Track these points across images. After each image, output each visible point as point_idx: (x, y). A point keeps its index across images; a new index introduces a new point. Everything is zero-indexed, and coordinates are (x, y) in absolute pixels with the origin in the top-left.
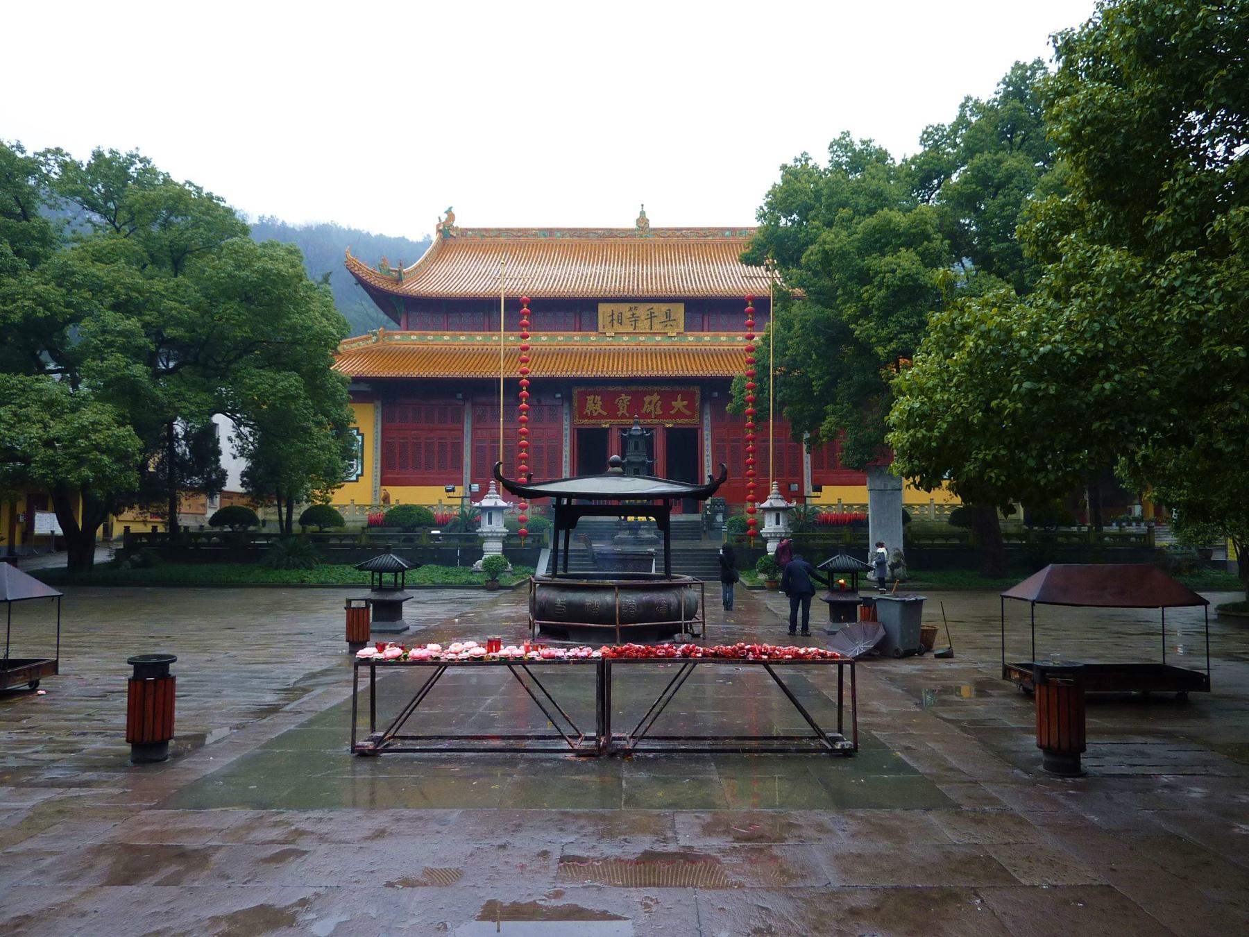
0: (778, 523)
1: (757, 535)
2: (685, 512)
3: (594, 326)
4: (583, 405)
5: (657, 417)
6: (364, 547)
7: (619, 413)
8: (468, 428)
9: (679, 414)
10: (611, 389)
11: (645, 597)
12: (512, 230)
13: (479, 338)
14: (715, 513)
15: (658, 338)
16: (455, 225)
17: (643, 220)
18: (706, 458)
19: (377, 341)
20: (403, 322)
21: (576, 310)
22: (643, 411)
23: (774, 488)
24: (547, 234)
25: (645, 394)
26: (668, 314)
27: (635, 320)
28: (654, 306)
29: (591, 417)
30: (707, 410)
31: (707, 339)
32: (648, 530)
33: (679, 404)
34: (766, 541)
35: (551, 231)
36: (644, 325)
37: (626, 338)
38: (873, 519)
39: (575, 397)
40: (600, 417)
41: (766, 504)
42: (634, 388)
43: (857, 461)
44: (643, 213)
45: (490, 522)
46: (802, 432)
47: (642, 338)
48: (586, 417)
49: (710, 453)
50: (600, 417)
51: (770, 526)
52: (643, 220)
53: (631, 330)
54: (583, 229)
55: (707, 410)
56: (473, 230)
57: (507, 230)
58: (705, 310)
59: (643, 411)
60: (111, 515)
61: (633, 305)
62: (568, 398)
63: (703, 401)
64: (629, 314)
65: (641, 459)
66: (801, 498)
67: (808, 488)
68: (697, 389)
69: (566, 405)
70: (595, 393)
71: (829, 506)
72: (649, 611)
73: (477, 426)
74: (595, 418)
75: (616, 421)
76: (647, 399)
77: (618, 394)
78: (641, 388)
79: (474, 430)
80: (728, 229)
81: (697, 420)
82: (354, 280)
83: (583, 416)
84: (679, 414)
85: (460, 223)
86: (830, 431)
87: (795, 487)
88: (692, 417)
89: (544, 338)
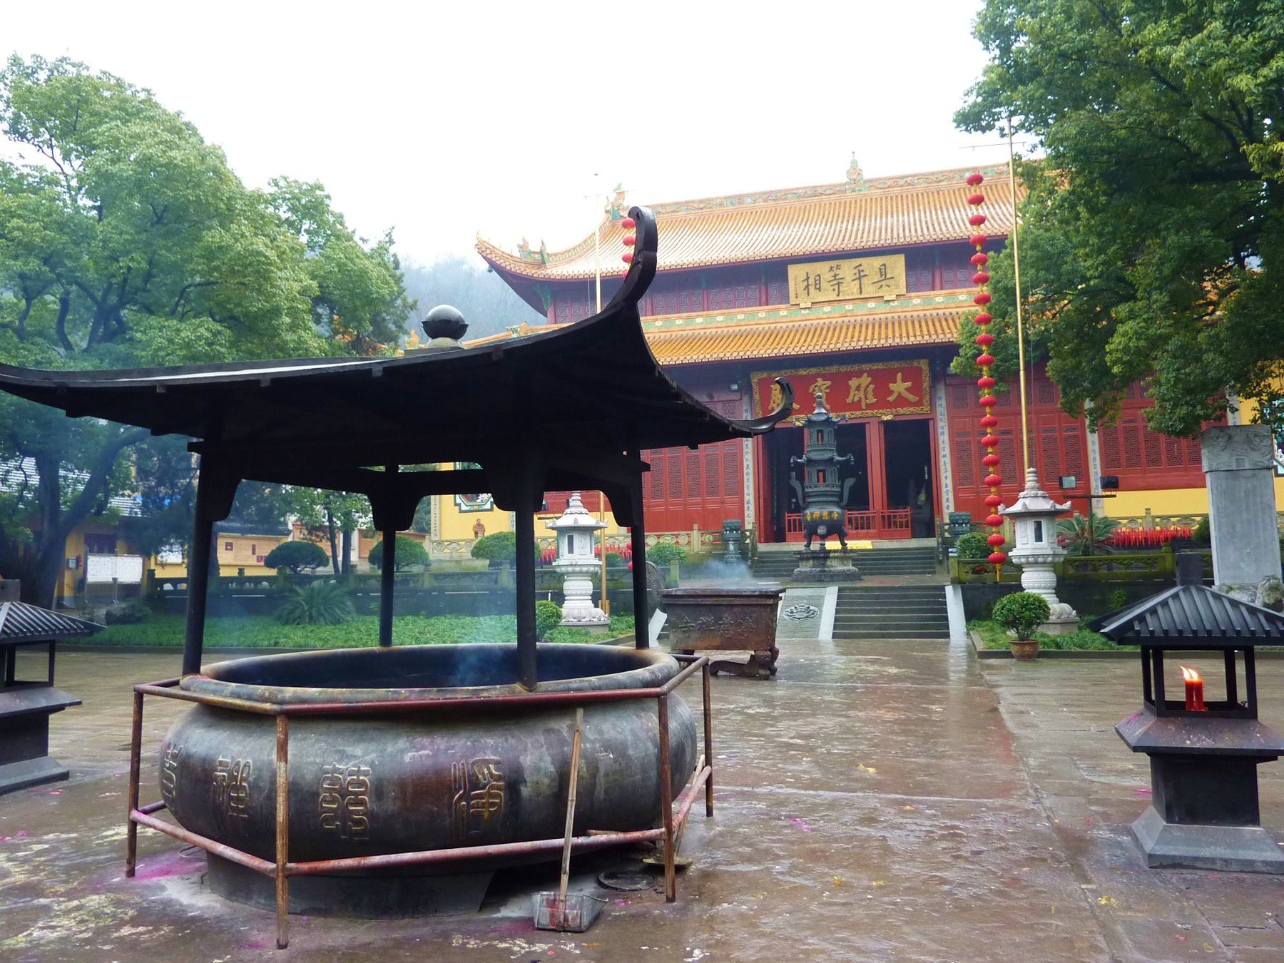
0: (1039, 538)
1: (1004, 560)
3: (784, 298)
5: (869, 407)
6: (428, 592)
9: (901, 401)
10: (803, 372)
11: (411, 753)
15: (871, 305)
17: (855, 170)
18: (942, 460)
22: (849, 400)
23: (1030, 478)
25: (850, 376)
26: (883, 271)
27: (838, 282)
28: (865, 262)
30: (941, 392)
32: (841, 559)
33: (899, 387)
35: (740, 198)
36: (850, 289)
37: (827, 309)
38: (1219, 527)
39: (755, 387)
41: (1017, 508)
42: (834, 369)
43: (1182, 419)
44: (854, 163)
45: (571, 550)
46: (1079, 399)
47: (849, 307)
51: (1024, 543)
52: (855, 170)
54: (780, 191)
55: (941, 392)
58: (931, 261)
59: (849, 400)
61: (834, 263)
62: (747, 389)
64: (829, 276)
65: (827, 456)
66: (1084, 500)
68: (924, 364)
69: (746, 399)
71: (1132, 520)
72: (425, 808)
76: (853, 383)
77: (812, 379)
78: (844, 369)
81: (927, 408)
82: (487, 265)
84: (901, 401)
86: (1126, 350)
87: (1070, 482)
88: (919, 404)
89: (720, 318)
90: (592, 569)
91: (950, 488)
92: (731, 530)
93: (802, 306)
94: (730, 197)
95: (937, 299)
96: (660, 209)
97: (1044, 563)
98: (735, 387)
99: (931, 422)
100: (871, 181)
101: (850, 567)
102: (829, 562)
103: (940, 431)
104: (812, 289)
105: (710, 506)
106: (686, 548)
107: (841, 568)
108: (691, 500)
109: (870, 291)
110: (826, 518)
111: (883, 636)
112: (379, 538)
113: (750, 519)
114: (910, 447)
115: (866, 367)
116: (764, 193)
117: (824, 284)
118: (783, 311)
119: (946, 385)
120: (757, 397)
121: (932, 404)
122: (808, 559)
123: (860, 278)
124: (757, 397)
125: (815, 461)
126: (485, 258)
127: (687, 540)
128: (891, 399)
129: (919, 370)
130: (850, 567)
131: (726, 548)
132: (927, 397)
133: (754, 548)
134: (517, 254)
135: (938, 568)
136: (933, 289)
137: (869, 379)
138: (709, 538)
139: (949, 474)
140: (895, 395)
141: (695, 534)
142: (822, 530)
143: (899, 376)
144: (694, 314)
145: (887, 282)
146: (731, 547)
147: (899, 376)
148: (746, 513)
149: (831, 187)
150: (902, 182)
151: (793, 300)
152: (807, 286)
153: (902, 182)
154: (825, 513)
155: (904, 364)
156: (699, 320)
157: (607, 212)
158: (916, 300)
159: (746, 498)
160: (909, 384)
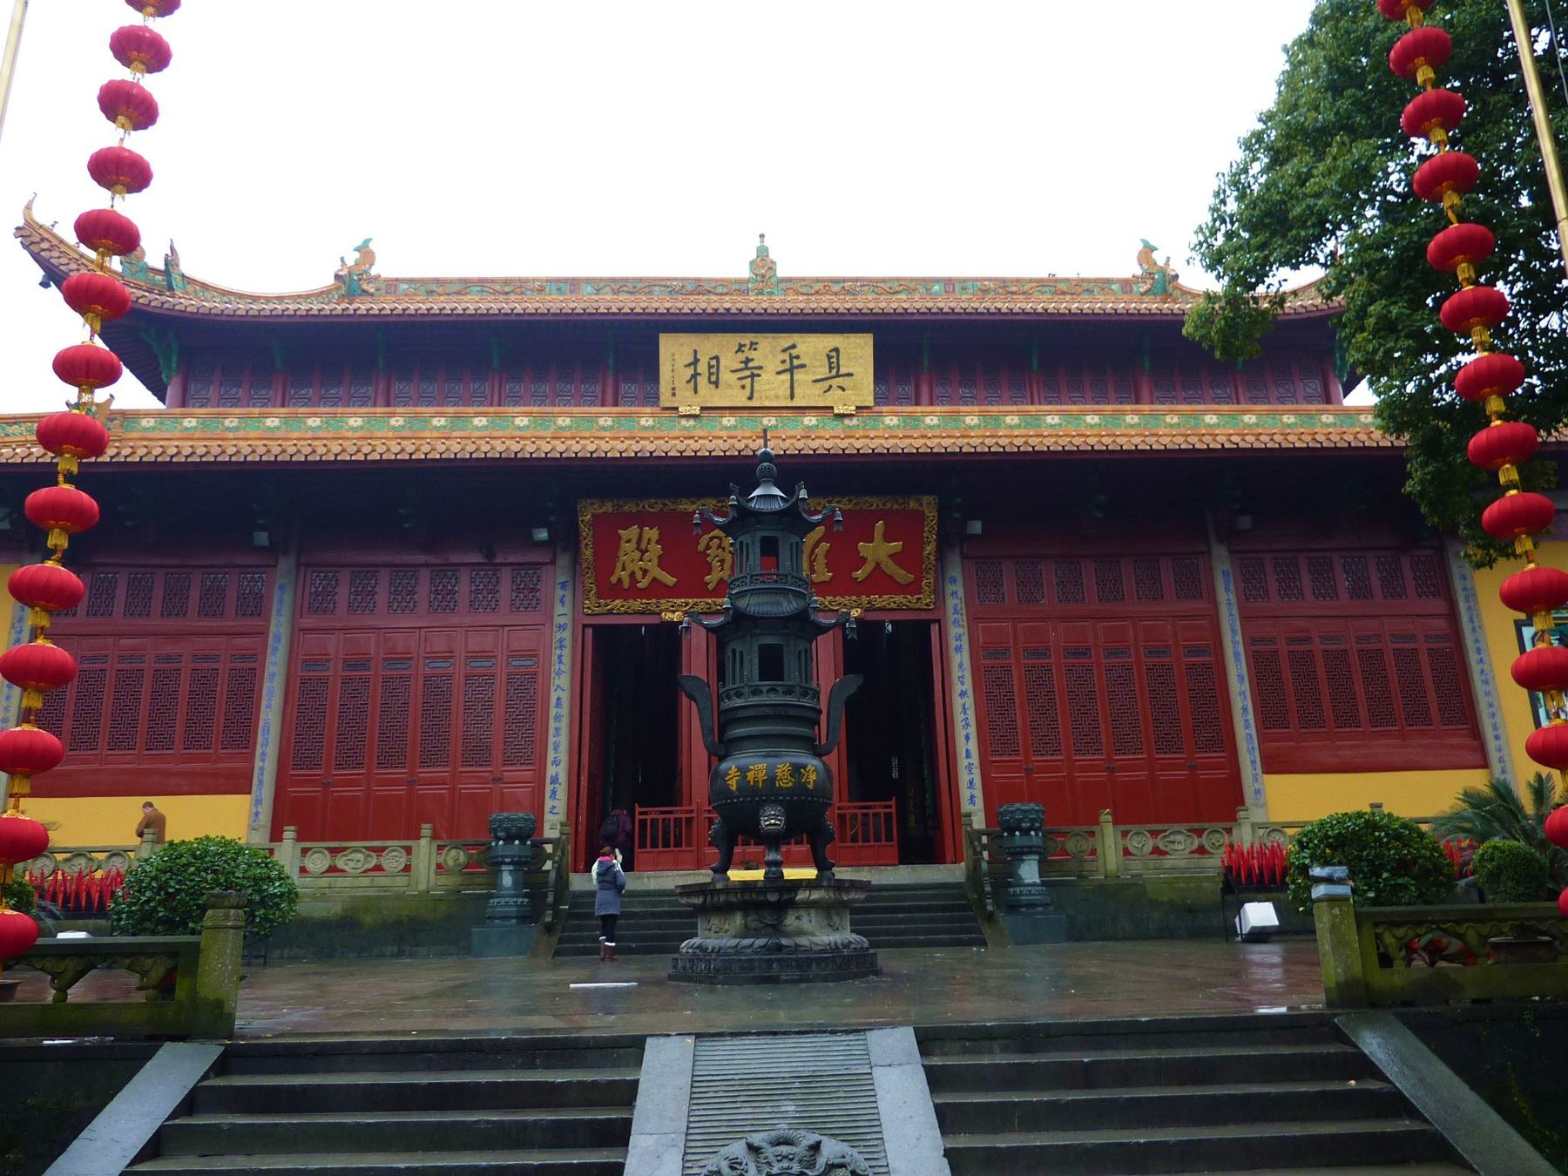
1: (1286, 972)
2: (903, 861)
7: (712, 579)
8: (279, 625)
9: (880, 581)
12: (493, 281)
13: (355, 422)
14: (1019, 854)
15: (810, 420)
26: (833, 356)
27: (751, 372)
29: (633, 592)
30: (955, 570)
31: (932, 421)
32: (827, 909)
33: (878, 550)
37: (729, 421)
39: (586, 532)
40: (657, 590)
44: (763, 252)
48: (617, 591)
49: (968, 685)
50: (657, 590)
54: (640, 280)
55: (955, 570)
56: (411, 281)
57: (481, 282)
60: (1106, 817)
61: (746, 339)
62: (565, 539)
63: (945, 542)
68: (928, 507)
69: (563, 560)
70: (643, 520)
79: (297, 632)
81: (927, 599)
82: (39, 273)
83: (609, 590)
84: (880, 581)
88: (913, 588)
89: (522, 422)
91: (975, 760)
92: (509, 839)
95: (928, 420)
96: (433, 287)
98: (542, 535)
99: (935, 629)
100: (789, 280)
101: (843, 935)
102: (790, 921)
103: (953, 644)
104: (702, 381)
105: (468, 787)
106: (401, 881)
107: (826, 938)
108: (424, 773)
109: (808, 394)
110: (785, 782)
112: (803, 913)
113: (555, 819)
114: (894, 674)
116: (614, 280)
117: (726, 376)
118: (646, 420)
119: (964, 557)
120: (588, 553)
121: (939, 592)
122: (726, 909)
123: (791, 370)
124: (588, 553)
126: (37, 257)
127: (403, 861)
128: (860, 574)
129: (920, 517)
130: (843, 935)
131: (494, 883)
133: (562, 881)
135: (987, 931)
136: (917, 403)
138: (455, 857)
139: (972, 730)
140: (869, 567)
141: (424, 847)
142: (771, 819)
144: (471, 409)
145: (839, 381)
146: (507, 880)
149: (723, 282)
150: (837, 288)
151: (666, 399)
152: (695, 376)
153: (837, 288)
154: (782, 767)
156: (480, 422)
157: (337, 277)
158: (890, 420)
159: (551, 770)
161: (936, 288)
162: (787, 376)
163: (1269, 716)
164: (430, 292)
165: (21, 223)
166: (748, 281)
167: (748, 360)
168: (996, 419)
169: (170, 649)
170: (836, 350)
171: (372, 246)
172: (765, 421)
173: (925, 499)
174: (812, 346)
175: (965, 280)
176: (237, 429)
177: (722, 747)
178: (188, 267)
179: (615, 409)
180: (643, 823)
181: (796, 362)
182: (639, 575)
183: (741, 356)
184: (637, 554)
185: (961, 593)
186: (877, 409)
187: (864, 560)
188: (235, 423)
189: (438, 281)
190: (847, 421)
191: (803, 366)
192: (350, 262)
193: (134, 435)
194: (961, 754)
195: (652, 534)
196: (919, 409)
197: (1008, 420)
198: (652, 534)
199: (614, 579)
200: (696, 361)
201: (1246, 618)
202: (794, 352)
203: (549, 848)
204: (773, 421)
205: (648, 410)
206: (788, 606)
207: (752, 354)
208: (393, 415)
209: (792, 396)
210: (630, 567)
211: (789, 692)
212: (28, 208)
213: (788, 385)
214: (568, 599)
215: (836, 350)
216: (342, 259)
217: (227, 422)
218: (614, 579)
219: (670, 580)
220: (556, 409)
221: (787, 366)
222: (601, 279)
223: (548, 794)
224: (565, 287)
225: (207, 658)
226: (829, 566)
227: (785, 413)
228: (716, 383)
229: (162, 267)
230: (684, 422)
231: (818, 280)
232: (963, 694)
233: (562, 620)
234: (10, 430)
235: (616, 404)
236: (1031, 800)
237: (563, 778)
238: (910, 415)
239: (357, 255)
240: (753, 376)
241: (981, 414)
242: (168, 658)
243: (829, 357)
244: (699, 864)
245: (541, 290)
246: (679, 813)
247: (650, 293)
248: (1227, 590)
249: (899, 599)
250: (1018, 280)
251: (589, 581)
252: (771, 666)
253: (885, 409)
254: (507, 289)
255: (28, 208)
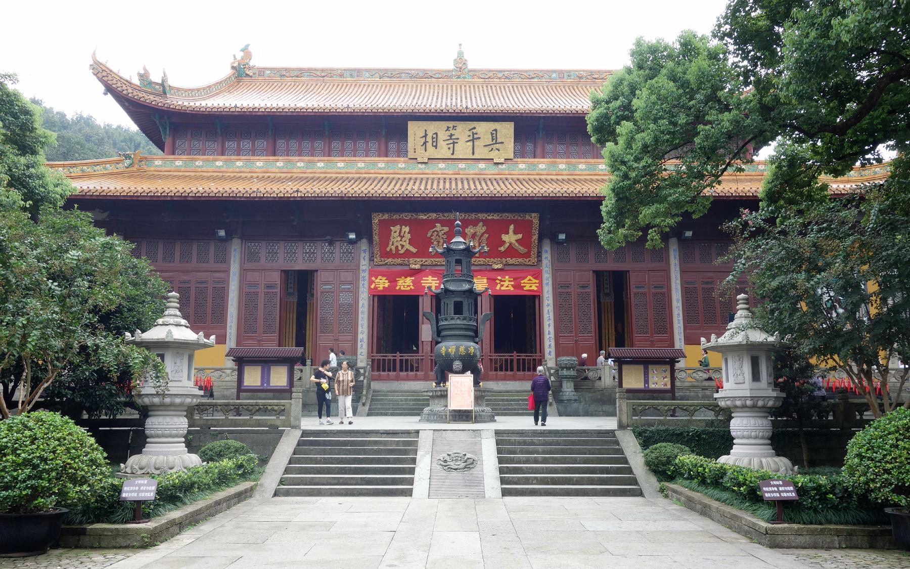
0: (756, 377)
3: (402, 152)
4: (386, 237)
15: (482, 165)
16: (251, 64)
17: (461, 61)
19: (131, 165)
20: (167, 147)
21: (385, 130)
24: (355, 74)
26: (494, 134)
27: (453, 141)
29: (397, 255)
33: (510, 238)
34: (728, 414)
36: (463, 149)
37: (442, 165)
39: (375, 228)
40: (408, 254)
44: (460, 54)
47: (462, 165)
48: (389, 255)
49: (551, 302)
52: (461, 61)
53: (448, 154)
54: (395, 70)
55: (547, 247)
57: (309, 70)
58: (539, 131)
61: (451, 124)
62: (365, 233)
67: (679, 342)
68: (534, 218)
70: (402, 223)
73: (248, 266)
74: (402, 256)
75: (429, 261)
77: (431, 224)
79: (243, 271)
80: (555, 71)
82: (102, 88)
85: (257, 61)
88: (527, 255)
90: (188, 400)
91: (552, 335)
93: (419, 160)
94: (351, 70)
95: (540, 166)
97: (744, 406)
104: (429, 145)
109: (481, 152)
111: (567, 493)
115: (482, 216)
117: (441, 143)
118: (401, 164)
120: (376, 238)
123: (473, 140)
125: (453, 292)
126: (101, 80)
128: (502, 249)
132: (536, 250)
134: (136, 81)
137: (484, 228)
140: (507, 245)
143: (512, 227)
145: (497, 146)
147: (512, 227)
148: (359, 351)
149: (439, 72)
151: (411, 154)
152: (425, 143)
153: (500, 75)
154: (462, 349)
155: (517, 217)
157: (233, 67)
158: (522, 165)
159: (360, 336)
160: (520, 236)
161: (554, 75)
162: (470, 144)
163: (688, 319)
164: (282, 76)
165: (92, 63)
166: (452, 71)
167: (451, 135)
168: (574, 165)
169: (185, 278)
170: (496, 130)
171: (250, 49)
172: (460, 166)
173: (533, 215)
174: (483, 128)
175: (569, 71)
176: (202, 166)
177: (440, 334)
178: (172, 82)
179: (385, 159)
180: (401, 361)
181: (476, 136)
182: (400, 248)
183: (448, 133)
184: (399, 239)
185: (549, 258)
186: (516, 160)
187: (504, 242)
188: (201, 163)
189: (287, 70)
190: (500, 166)
191: (479, 138)
192: (239, 57)
193: (152, 169)
194: (546, 332)
195: (407, 229)
196: (536, 160)
197: (580, 166)
198: (407, 229)
199: (388, 249)
200: (426, 136)
201: (683, 272)
202: (475, 131)
203: (362, 371)
204: (464, 166)
205: (402, 159)
206: (466, 287)
207: (453, 132)
208: (278, 160)
209: (473, 154)
210: (396, 244)
211: (464, 319)
212: (94, 54)
213: (471, 148)
214: (367, 258)
215: (496, 130)
216: (234, 56)
217: (197, 163)
218: (388, 249)
219: (414, 250)
220: (357, 158)
221: (471, 138)
222: (374, 70)
223: (359, 346)
224: (355, 74)
225: (202, 282)
226: (488, 245)
227: (469, 162)
228: (436, 147)
229: (160, 82)
230: (420, 165)
231: (490, 71)
232: (548, 305)
233: (364, 267)
234: (95, 168)
235: (387, 156)
236: (573, 355)
237: (366, 340)
238: (532, 164)
239: (242, 54)
240: (454, 143)
241: (567, 163)
242: (184, 282)
243: (492, 134)
244: (426, 378)
245: (341, 75)
246: (418, 356)
247: (400, 77)
248: (675, 258)
249: (520, 260)
250: (599, 71)
251: (377, 250)
252: (458, 309)
253: (519, 160)
254: (323, 74)
255: (94, 54)
